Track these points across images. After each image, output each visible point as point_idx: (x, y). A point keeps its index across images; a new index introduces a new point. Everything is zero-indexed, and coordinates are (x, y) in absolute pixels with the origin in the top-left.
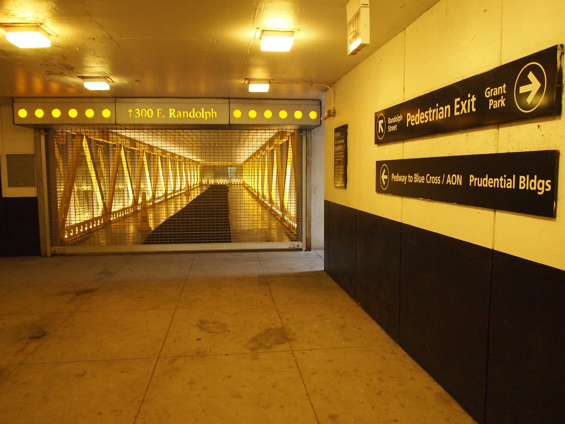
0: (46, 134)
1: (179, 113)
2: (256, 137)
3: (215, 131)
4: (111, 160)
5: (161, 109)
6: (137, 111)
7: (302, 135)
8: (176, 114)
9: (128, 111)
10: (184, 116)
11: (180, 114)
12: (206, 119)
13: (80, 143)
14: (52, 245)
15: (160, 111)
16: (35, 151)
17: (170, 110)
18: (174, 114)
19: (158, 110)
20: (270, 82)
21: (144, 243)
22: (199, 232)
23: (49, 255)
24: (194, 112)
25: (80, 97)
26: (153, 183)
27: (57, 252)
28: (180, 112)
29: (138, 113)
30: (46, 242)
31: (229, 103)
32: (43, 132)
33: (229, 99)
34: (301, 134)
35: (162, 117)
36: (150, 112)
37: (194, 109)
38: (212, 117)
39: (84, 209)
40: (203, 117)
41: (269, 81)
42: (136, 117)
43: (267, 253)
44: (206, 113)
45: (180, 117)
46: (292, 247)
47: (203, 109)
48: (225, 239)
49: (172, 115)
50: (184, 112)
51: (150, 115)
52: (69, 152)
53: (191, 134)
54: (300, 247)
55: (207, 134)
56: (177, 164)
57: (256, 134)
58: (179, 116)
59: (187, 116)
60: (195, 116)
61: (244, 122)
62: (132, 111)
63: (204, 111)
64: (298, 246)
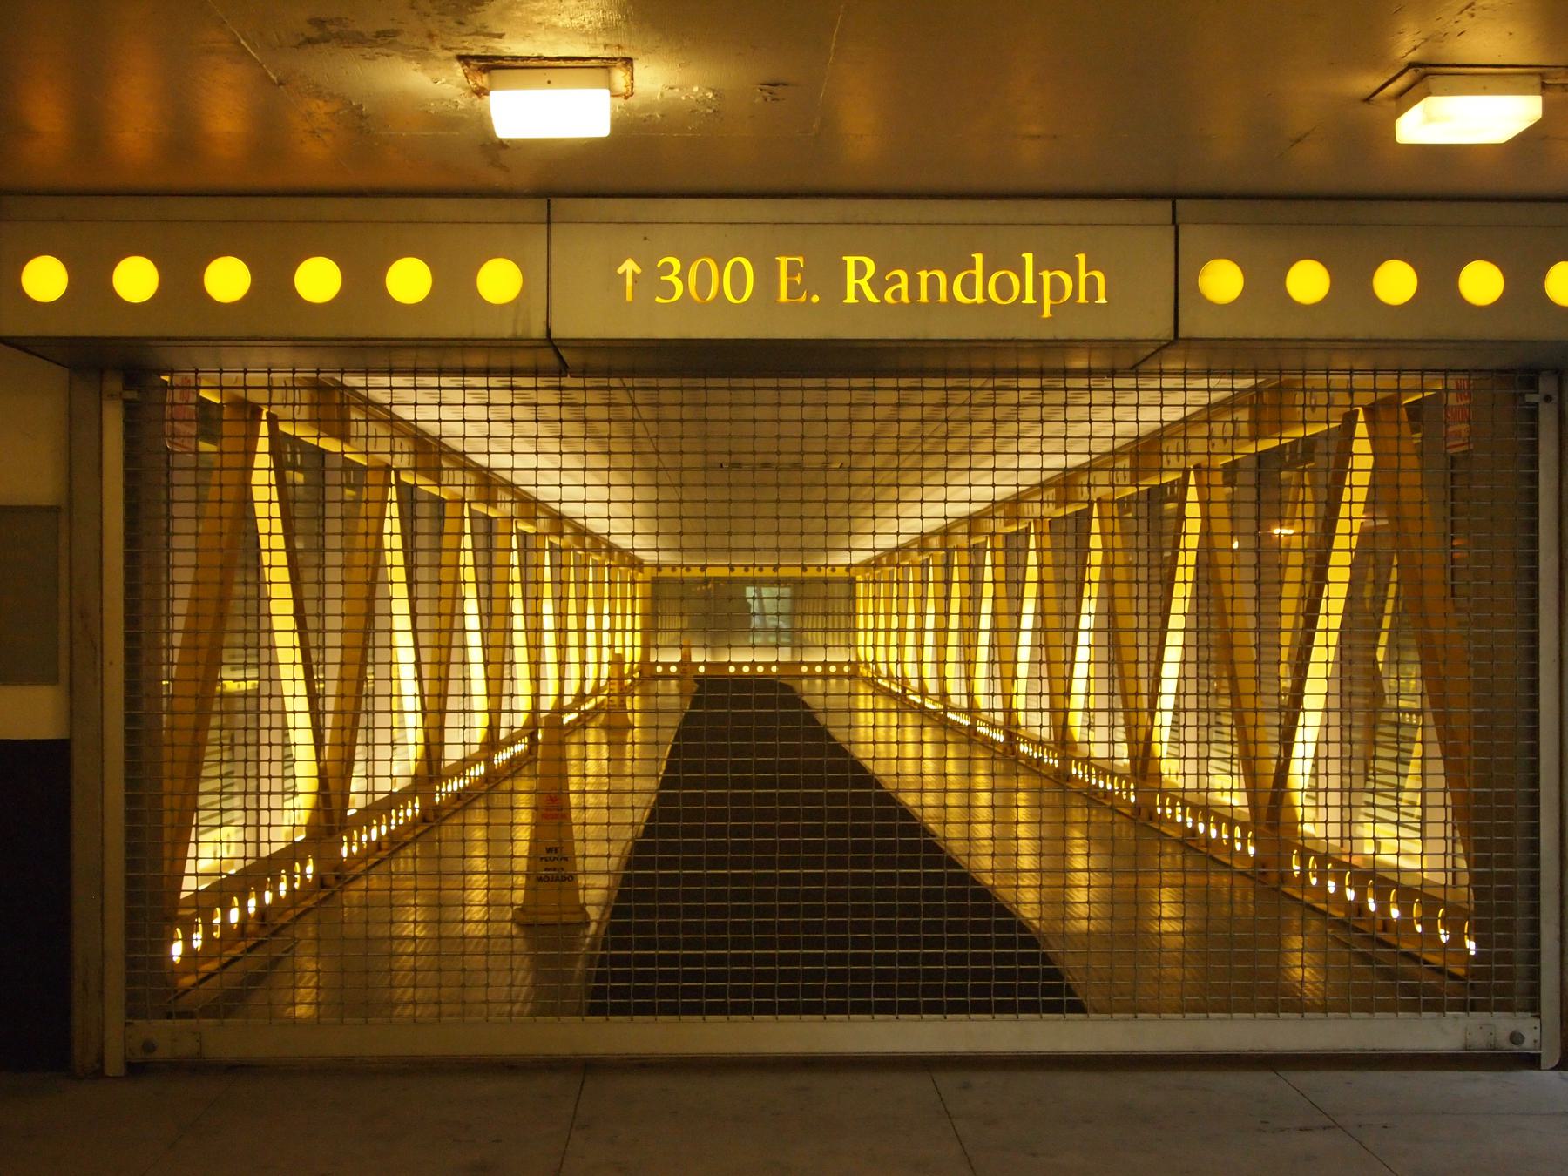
0: (131, 395)
1: (897, 280)
2: (867, 413)
3: (687, 382)
4: (333, 542)
5: (801, 260)
6: (668, 268)
7: (1537, 404)
8: (879, 284)
9: (620, 270)
10: (924, 298)
11: (903, 286)
12: (1047, 313)
13: (239, 445)
14: (133, 1013)
15: (793, 269)
16: (70, 490)
17: (850, 261)
18: (870, 282)
19: (783, 262)
20: (1544, 86)
21: (595, 1010)
22: (951, 946)
23: (114, 1066)
24: (978, 272)
25: (274, 194)
26: (427, 671)
27: (163, 1052)
28: (903, 274)
29: (672, 278)
30: (101, 993)
31: (549, 222)
32: (114, 384)
33: (1173, 197)
34: (1532, 398)
35: (803, 299)
36: (738, 271)
37: (979, 258)
38: (1082, 299)
39: (222, 810)
40: (1029, 299)
41: (1541, 74)
42: (658, 300)
43: (1349, 1075)
44: (1046, 276)
45: (905, 298)
46: (1479, 1041)
47: (1029, 258)
48: (977, 991)
49: (859, 291)
50: (924, 275)
51: (738, 292)
52: (178, 493)
53: (505, 397)
54: (1528, 1045)
55: (593, 397)
56: (547, 562)
57: (870, 397)
58: (896, 294)
59: (943, 297)
60: (985, 294)
61: (1260, 327)
62: (638, 270)
63: (1037, 269)
64: (1515, 1038)
